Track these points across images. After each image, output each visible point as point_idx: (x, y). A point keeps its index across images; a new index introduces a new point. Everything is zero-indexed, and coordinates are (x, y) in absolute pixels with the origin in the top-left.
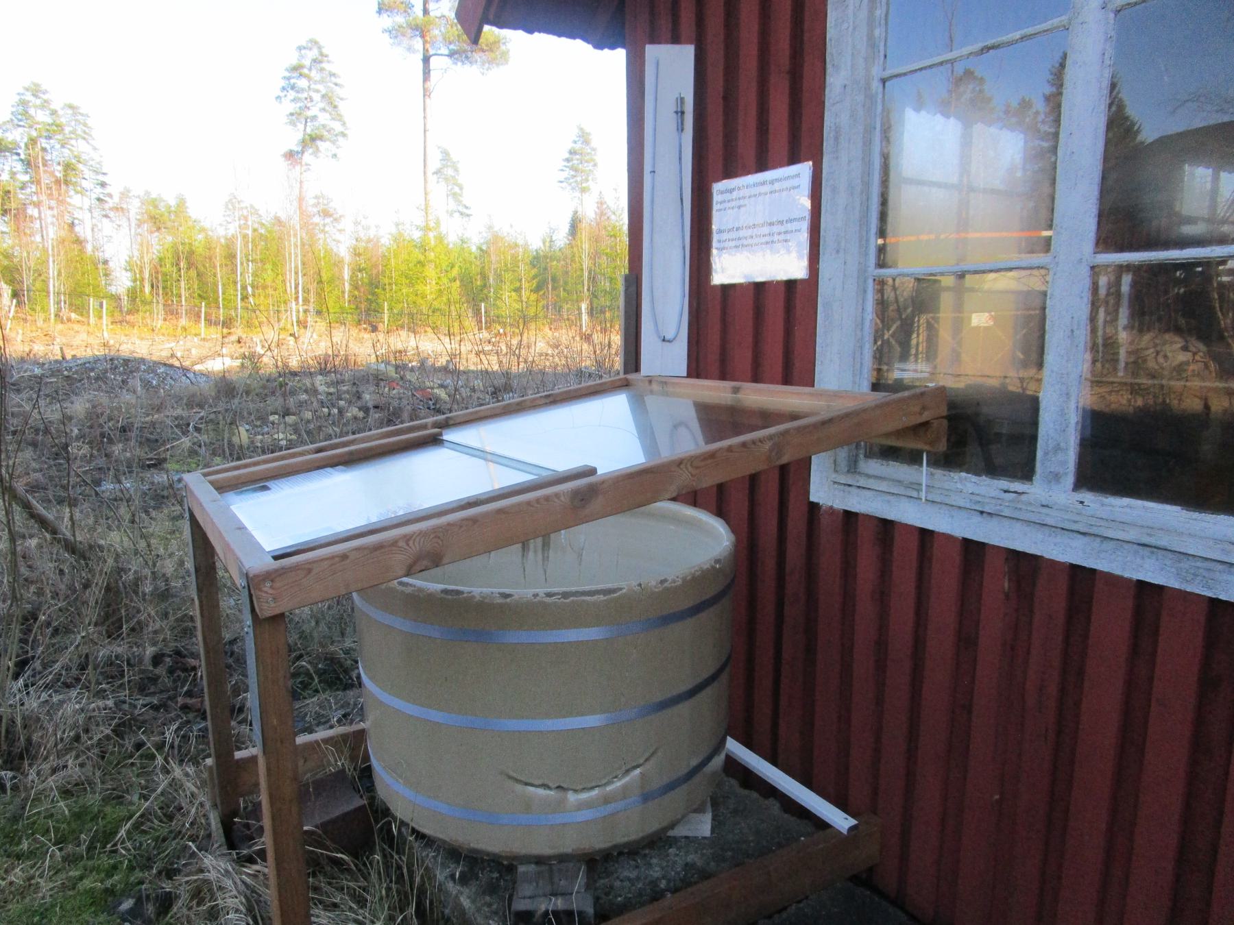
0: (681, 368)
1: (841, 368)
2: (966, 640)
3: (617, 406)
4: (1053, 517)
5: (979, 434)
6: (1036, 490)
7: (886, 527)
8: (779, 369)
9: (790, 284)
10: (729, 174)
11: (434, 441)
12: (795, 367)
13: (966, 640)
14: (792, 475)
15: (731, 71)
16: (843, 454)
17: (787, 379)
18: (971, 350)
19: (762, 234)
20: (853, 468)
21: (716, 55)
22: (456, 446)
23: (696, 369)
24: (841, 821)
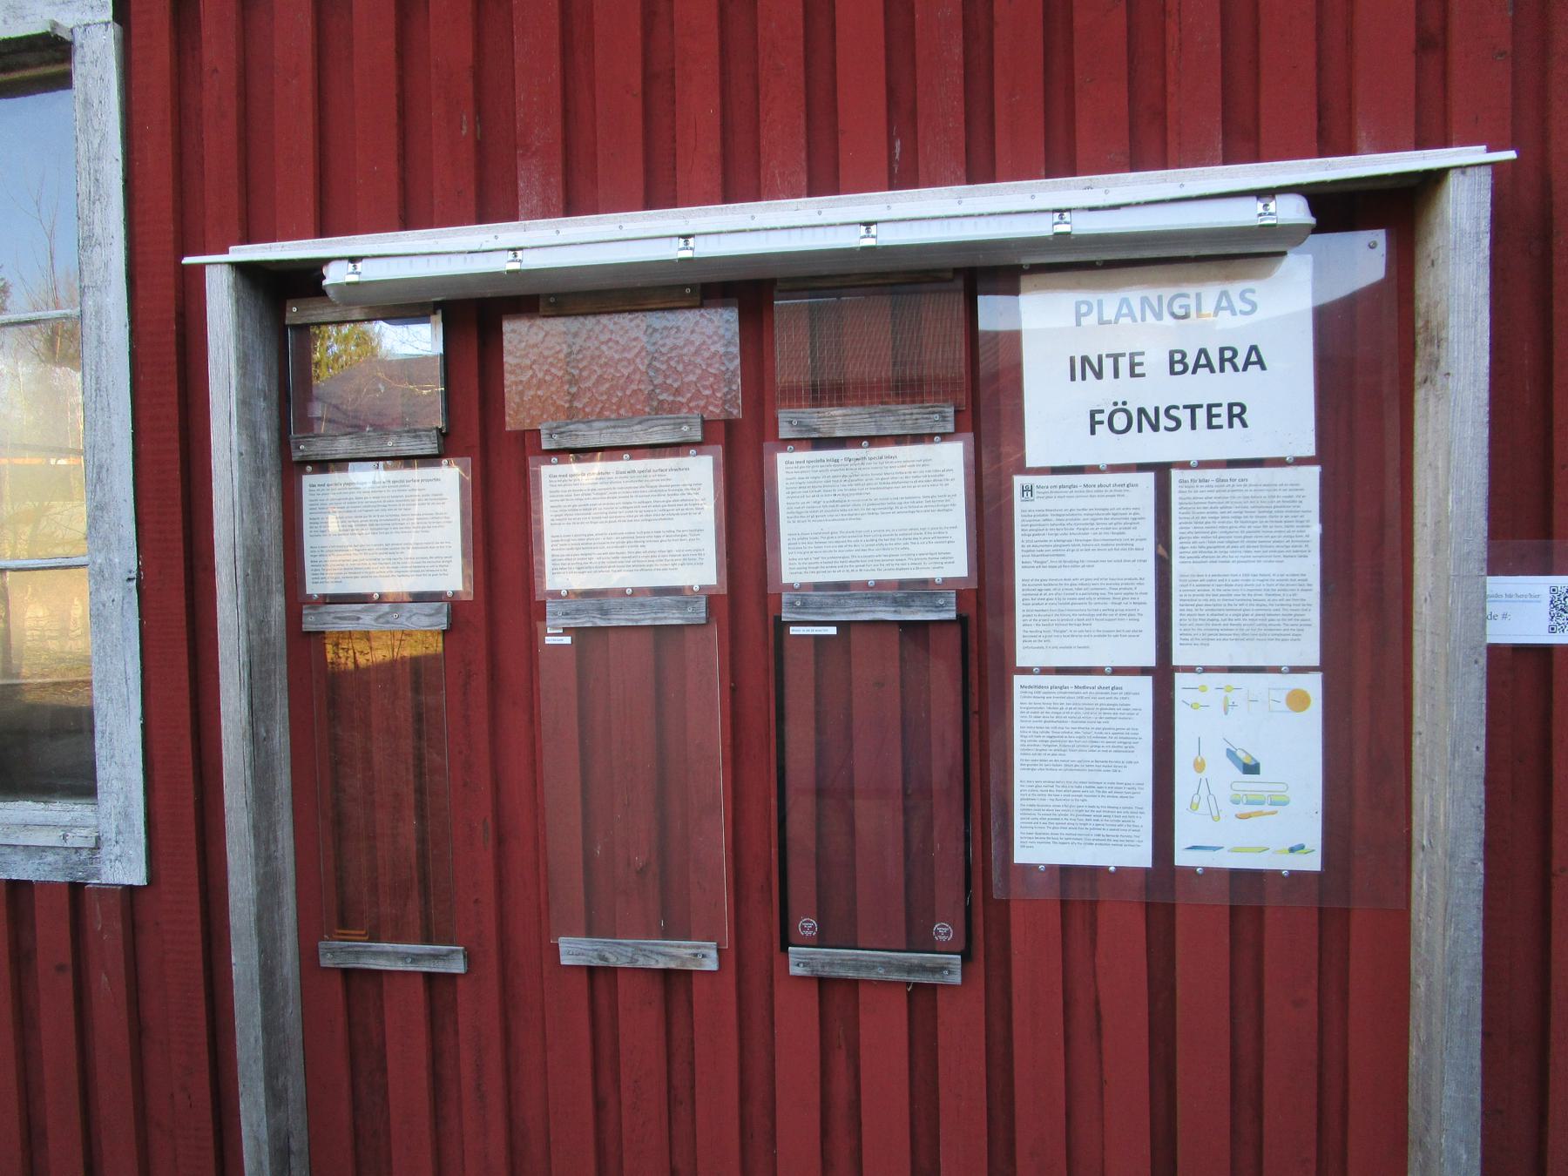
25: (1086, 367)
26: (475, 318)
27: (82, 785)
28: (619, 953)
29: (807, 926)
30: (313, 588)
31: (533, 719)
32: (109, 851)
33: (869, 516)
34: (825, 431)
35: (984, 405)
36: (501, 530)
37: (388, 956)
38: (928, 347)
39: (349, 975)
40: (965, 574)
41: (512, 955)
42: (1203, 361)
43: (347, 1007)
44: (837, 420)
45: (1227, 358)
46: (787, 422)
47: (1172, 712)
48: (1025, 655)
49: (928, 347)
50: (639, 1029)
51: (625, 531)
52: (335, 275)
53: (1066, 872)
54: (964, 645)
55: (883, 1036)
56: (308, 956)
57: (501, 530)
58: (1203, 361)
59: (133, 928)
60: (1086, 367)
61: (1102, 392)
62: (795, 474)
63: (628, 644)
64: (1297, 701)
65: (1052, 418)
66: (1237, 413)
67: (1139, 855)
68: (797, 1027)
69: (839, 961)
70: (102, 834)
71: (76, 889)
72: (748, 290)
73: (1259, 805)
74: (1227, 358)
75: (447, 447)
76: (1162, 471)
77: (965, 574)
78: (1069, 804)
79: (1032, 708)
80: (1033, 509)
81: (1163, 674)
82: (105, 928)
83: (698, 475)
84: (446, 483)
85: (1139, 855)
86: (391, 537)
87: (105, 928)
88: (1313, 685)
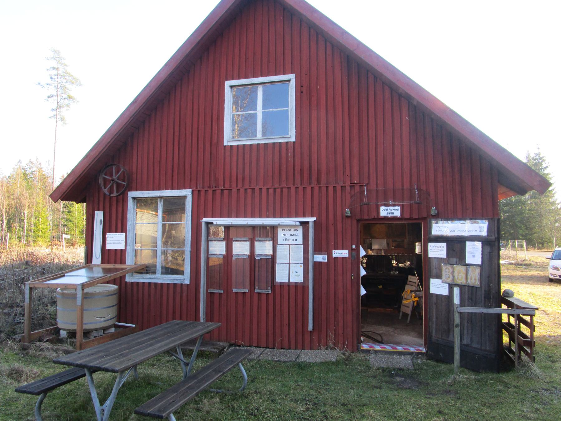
0: (100, 263)
1: (130, 261)
2: (149, 296)
3: (83, 272)
4: (159, 278)
5: (147, 269)
6: (157, 275)
7: (138, 283)
8: (405, 207)
9: (121, 250)
10: (110, 232)
11: (64, 276)
12: (123, 261)
13: (149, 296)
14: (122, 278)
15: (110, 221)
16: (131, 274)
17: (121, 263)
18: (145, 258)
19: (115, 241)
20: (132, 275)
21: (108, 215)
22: (70, 276)
23: (103, 262)
24: (134, 326)
25: (284, 235)
26: (227, 228)
27: (182, 273)
28: (238, 290)
29: (257, 287)
30: (210, 253)
31: (231, 267)
32: (186, 280)
33: (264, 248)
34: (370, 131)
35: (274, 239)
36: (229, 248)
37: (215, 291)
38: (270, 233)
39: (211, 293)
40: (431, 279)
41: (228, 290)
42: (293, 235)
43: (210, 296)
44: (261, 239)
45: (295, 235)
46: (256, 239)
47: (291, 268)
48: (277, 262)
49: (270, 233)
50: (240, 298)
51: (241, 248)
52: (214, 223)
53: (281, 282)
54: (272, 261)
55: (264, 298)
56: (207, 291)
57: (229, 248)
58: (293, 235)
59: (188, 288)
60: (284, 235)
61: (286, 237)
62: (257, 244)
63: (241, 260)
64: (301, 266)
65: (280, 239)
66: (296, 240)
67: (287, 281)
68: (256, 298)
69: (260, 291)
70: (185, 279)
71: (182, 284)
72: (254, 227)
73: (297, 277)
74: (295, 235)
75: (224, 239)
76: (290, 245)
77: (431, 279)
78: (281, 277)
79: (278, 267)
80: (278, 248)
81: (289, 264)
82: (185, 289)
83: (248, 243)
84: (223, 243)
85: (287, 281)
86: (218, 248)
87: (185, 289)
88: (302, 265)
